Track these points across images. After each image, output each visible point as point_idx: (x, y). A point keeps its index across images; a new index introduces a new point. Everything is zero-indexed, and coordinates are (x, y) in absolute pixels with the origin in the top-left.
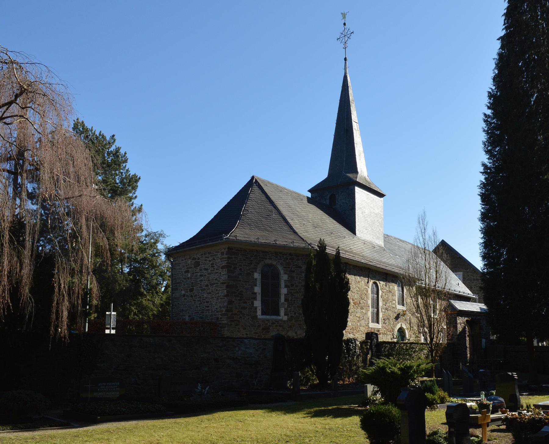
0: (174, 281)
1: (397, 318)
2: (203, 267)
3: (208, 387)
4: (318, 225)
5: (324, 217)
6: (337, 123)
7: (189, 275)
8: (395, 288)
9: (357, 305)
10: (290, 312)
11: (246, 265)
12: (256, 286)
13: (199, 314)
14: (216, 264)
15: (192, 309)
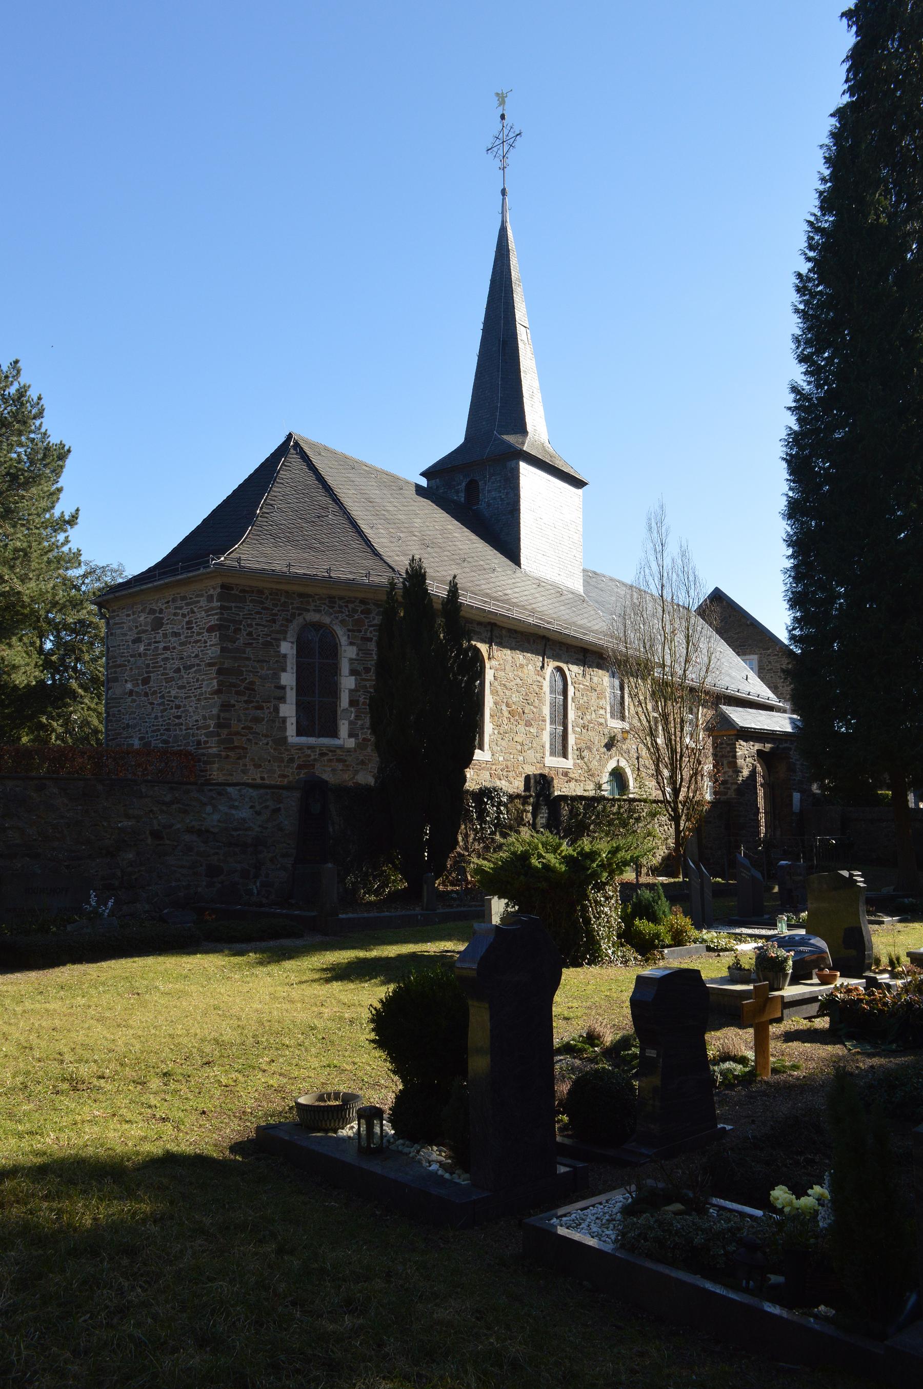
0: (110, 661)
1: (609, 746)
2: (168, 628)
3: (113, 901)
4: (433, 543)
5: (449, 527)
6: (485, 330)
7: (142, 649)
8: (603, 680)
9: (517, 718)
10: (362, 729)
11: (263, 625)
12: (284, 670)
13: (161, 735)
14: (196, 622)
15: (146, 722)
